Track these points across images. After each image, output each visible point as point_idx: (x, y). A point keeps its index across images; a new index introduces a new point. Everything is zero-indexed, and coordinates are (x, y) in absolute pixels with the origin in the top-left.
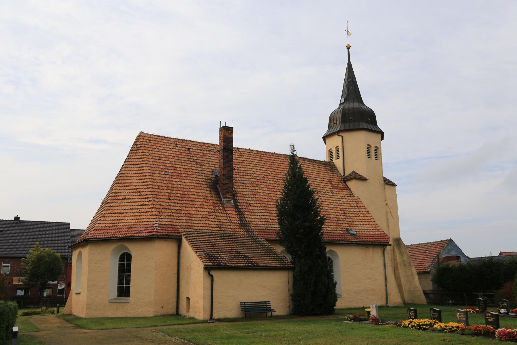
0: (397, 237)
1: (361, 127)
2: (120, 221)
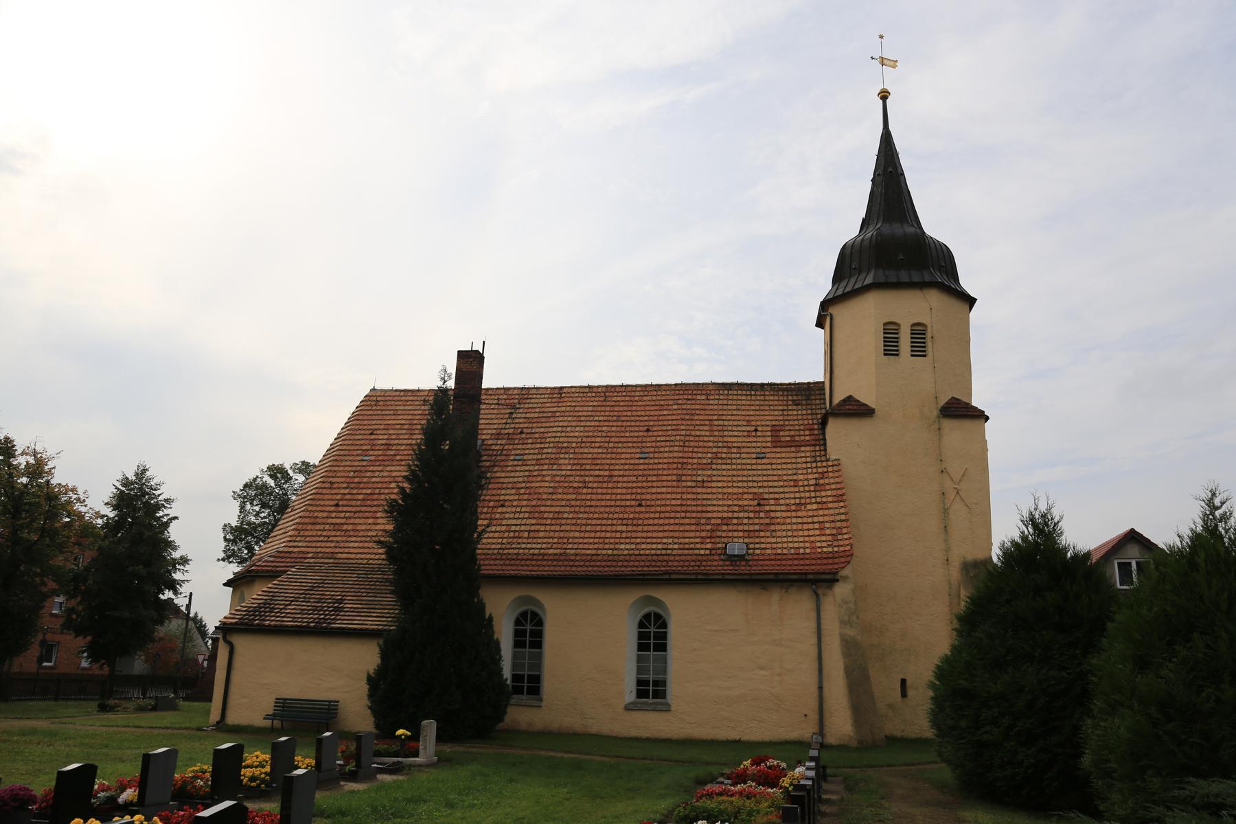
1: (927, 278)
2: (650, 535)
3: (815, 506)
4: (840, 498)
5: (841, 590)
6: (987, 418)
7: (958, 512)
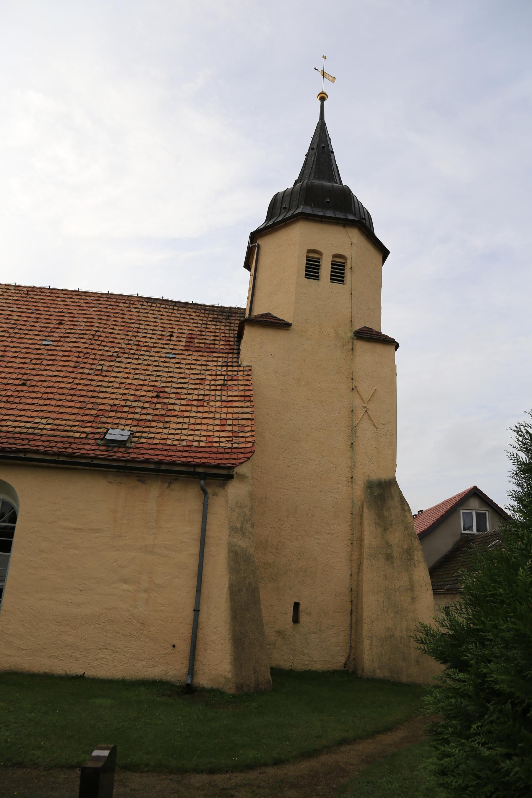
0: (384, 476)
2: (23, 413)
3: (219, 404)
4: (247, 398)
5: (235, 490)
6: (397, 346)
7: (365, 429)
